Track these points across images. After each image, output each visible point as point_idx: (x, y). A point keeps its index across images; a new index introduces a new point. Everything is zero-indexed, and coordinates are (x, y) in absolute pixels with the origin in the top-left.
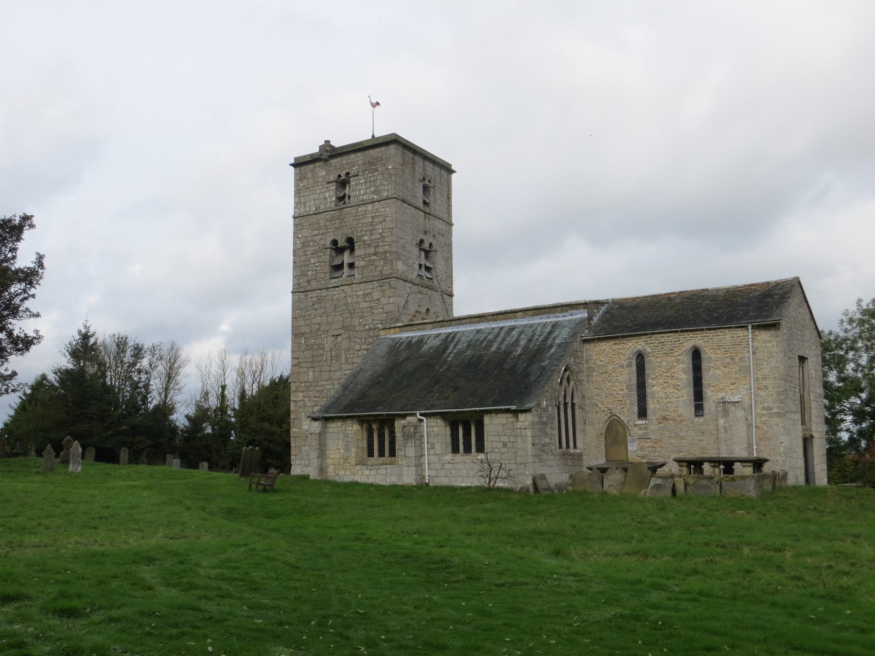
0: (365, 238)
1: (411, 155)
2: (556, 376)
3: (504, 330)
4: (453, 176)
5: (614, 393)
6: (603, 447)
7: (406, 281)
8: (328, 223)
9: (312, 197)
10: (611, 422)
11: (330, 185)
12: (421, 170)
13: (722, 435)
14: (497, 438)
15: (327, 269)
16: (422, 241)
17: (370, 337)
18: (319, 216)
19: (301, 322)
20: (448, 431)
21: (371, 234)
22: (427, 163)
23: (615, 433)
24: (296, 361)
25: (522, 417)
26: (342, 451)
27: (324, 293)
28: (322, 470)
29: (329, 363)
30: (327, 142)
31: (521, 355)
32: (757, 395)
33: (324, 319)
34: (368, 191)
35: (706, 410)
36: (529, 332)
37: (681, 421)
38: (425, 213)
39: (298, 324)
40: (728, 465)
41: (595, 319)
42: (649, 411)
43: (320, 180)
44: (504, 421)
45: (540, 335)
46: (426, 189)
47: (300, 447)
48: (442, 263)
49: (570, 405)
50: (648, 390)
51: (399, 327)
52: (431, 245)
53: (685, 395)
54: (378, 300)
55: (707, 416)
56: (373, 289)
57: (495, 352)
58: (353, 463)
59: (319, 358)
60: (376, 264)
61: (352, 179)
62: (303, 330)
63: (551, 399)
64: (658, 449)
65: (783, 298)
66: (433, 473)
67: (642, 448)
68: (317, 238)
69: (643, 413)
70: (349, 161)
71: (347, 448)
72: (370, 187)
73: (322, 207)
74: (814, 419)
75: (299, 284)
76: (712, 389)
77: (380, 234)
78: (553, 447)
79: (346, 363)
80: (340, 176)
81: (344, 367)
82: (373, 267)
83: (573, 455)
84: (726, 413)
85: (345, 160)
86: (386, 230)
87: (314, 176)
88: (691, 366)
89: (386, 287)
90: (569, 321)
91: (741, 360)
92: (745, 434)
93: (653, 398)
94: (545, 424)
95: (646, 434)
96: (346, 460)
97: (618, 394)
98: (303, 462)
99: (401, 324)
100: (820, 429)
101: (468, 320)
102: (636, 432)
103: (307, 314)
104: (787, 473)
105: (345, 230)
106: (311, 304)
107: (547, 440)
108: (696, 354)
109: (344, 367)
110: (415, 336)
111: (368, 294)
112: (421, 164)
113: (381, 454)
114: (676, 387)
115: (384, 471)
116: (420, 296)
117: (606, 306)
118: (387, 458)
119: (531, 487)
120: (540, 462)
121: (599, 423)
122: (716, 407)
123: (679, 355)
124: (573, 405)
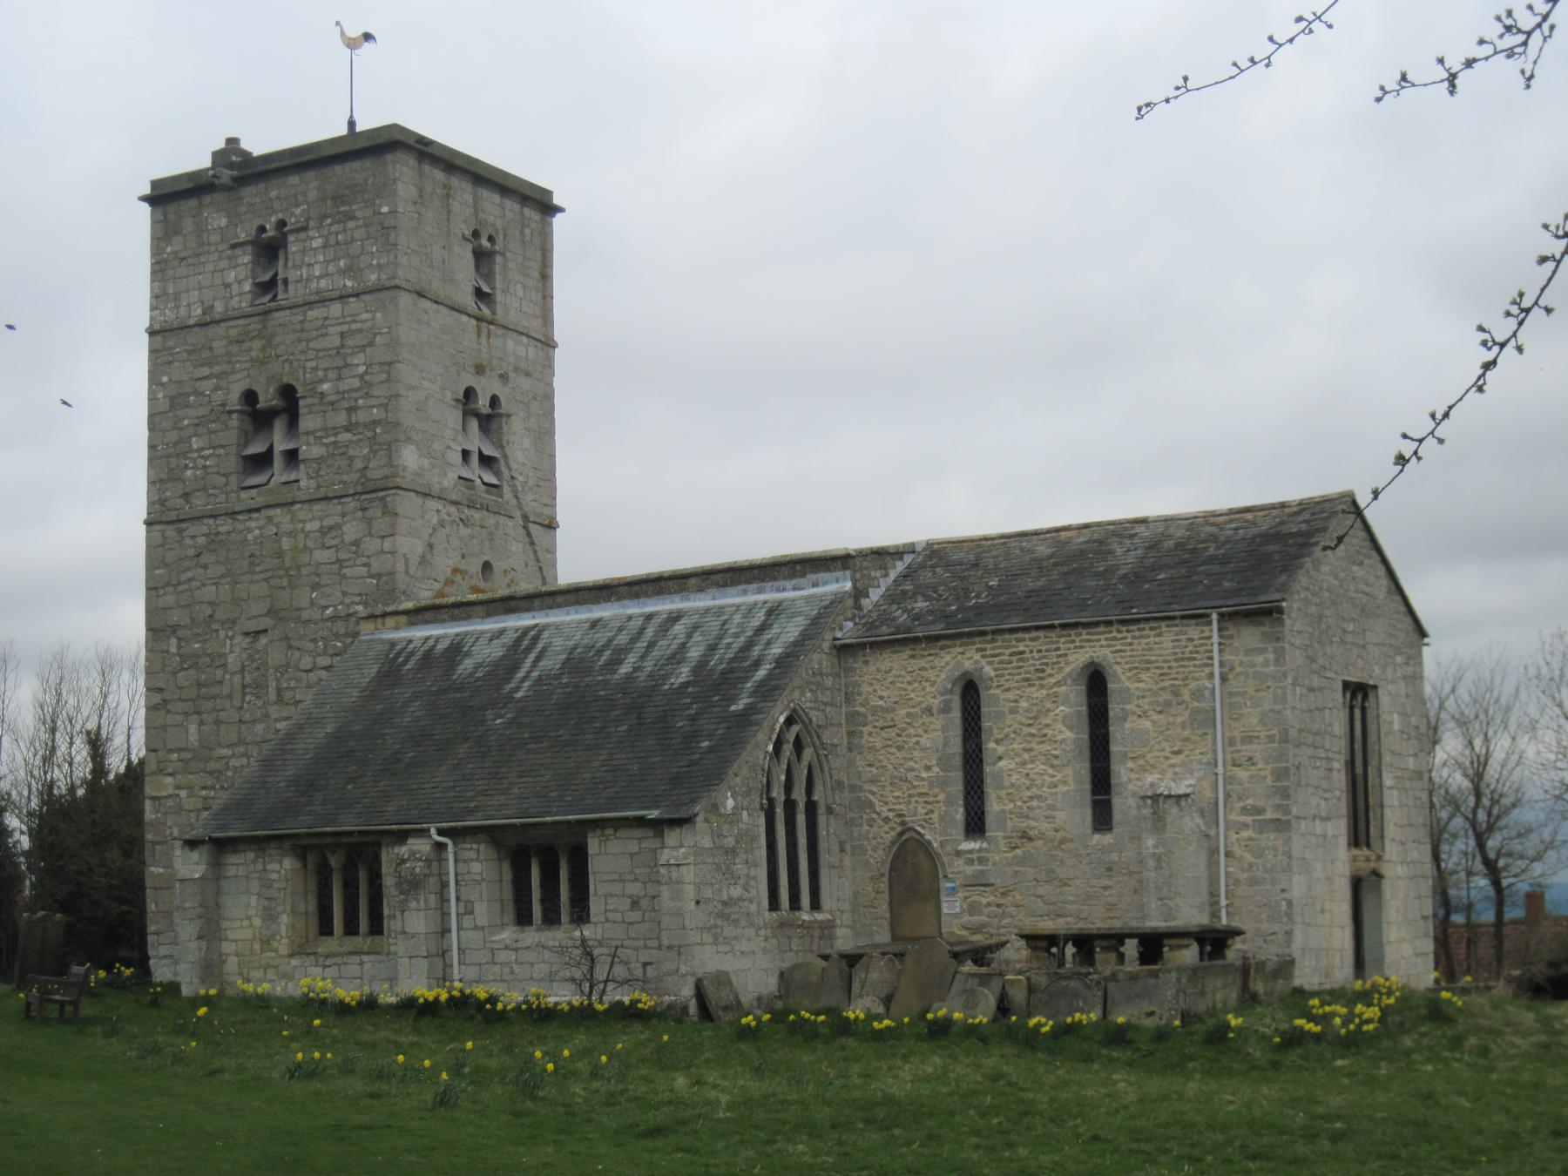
0: (325, 387)
1: (439, 175)
2: (761, 737)
3: (656, 621)
4: (558, 220)
5: (910, 776)
6: (885, 907)
7: (426, 495)
8: (234, 349)
9: (193, 281)
10: (903, 846)
11: (238, 251)
12: (469, 212)
14: (616, 888)
15: (232, 464)
16: (469, 393)
17: (337, 636)
18: (211, 331)
19: (169, 599)
20: (508, 875)
21: (339, 378)
22: (485, 193)
23: (911, 871)
24: (157, 698)
25: (672, 837)
26: (257, 922)
27: (224, 526)
28: (210, 969)
30: (232, 142)
31: (686, 685)
32: (1229, 780)
34: (331, 269)
35: (1117, 816)
36: (714, 625)
37: (1063, 841)
38: (479, 319)
39: (161, 603)
40: (1152, 946)
41: (875, 595)
42: (990, 819)
43: (214, 238)
44: (633, 847)
45: (736, 635)
46: (482, 258)
48: (526, 443)
49: (801, 806)
50: (987, 769)
51: (406, 612)
52: (494, 401)
53: (1070, 779)
54: (356, 543)
55: (1117, 830)
57: (629, 678)
58: (283, 950)
59: (215, 690)
60: (351, 452)
61: (291, 238)
62: (175, 617)
63: (748, 794)
65: (1303, 545)
66: (471, 972)
67: (973, 909)
69: (976, 824)
70: (284, 192)
71: (269, 916)
72: (336, 259)
73: (219, 307)
74: (1391, 831)
75: (162, 502)
76: (1130, 765)
77: (361, 377)
78: (753, 908)
79: (280, 700)
80: (262, 229)
81: (274, 712)
82: (344, 462)
84: (1158, 821)
85: (275, 190)
86: (376, 368)
87: (200, 229)
88: (1084, 709)
89: (375, 512)
94: (731, 852)
95: (982, 872)
96: (266, 942)
97: (918, 778)
99: (410, 605)
100: (1415, 855)
101: (572, 597)
102: (958, 869)
103: (184, 577)
104: (1292, 962)
105: (275, 367)
107: (736, 892)
108: (1096, 683)
109: (274, 712)
110: (444, 637)
111: (331, 528)
112: (469, 198)
113: (351, 929)
114: (1049, 760)
116: (465, 532)
117: (908, 559)
120: (715, 943)
121: (875, 849)
122: (1139, 808)
123: (1058, 684)
124: (811, 807)
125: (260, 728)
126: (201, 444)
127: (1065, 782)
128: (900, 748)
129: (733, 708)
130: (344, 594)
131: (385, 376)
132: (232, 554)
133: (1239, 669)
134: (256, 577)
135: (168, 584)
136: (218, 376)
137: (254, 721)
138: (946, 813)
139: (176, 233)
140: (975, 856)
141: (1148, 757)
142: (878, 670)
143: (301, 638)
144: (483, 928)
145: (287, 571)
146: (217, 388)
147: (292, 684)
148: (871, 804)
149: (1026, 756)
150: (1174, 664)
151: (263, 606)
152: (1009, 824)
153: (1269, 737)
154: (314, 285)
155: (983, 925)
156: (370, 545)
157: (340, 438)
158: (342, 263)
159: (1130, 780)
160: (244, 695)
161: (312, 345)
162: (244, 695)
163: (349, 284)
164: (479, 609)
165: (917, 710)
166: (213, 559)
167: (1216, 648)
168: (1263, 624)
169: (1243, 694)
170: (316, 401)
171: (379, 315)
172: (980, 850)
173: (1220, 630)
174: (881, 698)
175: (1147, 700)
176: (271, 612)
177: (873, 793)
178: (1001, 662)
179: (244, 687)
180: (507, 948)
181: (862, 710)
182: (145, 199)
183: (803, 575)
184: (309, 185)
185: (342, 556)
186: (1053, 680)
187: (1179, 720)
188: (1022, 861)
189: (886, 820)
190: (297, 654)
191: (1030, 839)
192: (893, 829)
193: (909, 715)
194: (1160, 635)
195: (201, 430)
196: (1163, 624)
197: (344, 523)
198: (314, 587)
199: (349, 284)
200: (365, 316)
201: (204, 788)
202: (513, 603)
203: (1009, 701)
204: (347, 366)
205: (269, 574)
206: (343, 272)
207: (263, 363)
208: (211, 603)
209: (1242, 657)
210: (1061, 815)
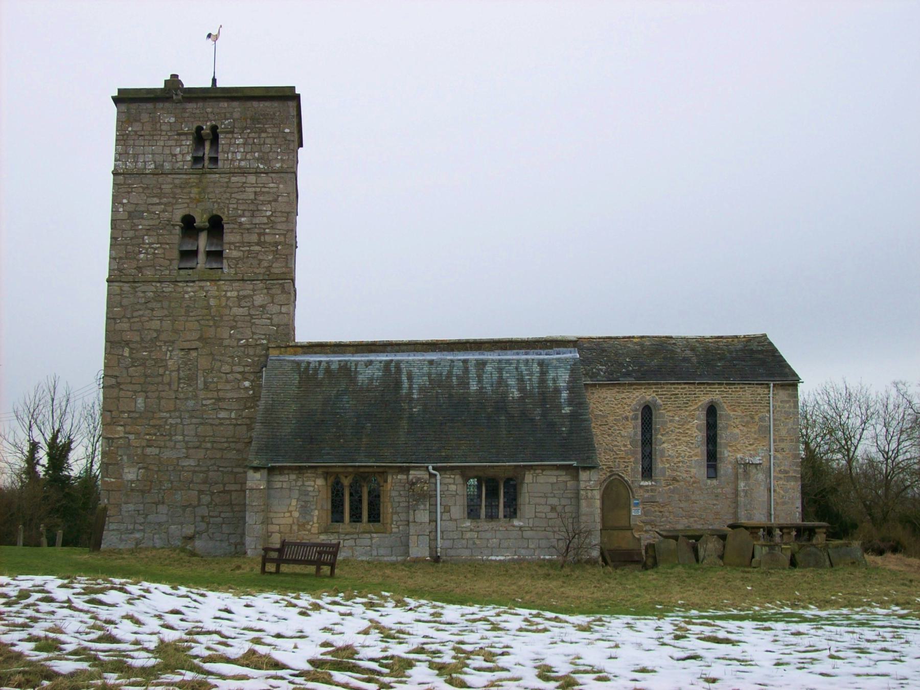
0: (243, 219)
5: (615, 449)
8: (179, 191)
10: (611, 482)
11: (183, 137)
13: (741, 499)
14: (543, 501)
15: (176, 254)
17: (248, 356)
21: (253, 216)
26: (296, 514)
29: (175, 387)
33: (167, 324)
37: (694, 482)
39: (118, 327)
47: (118, 506)
56: (254, 290)
58: (314, 530)
66: (448, 543)
68: (158, 209)
69: (647, 472)
71: (305, 509)
72: (252, 152)
73: (167, 166)
75: (120, 270)
76: (729, 449)
77: (268, 217)
79: (206, 387)
81: (202, 394)
82: (255, 262)
87: (155, 121)
89: (276, 290)
92: (765, 498)
93: (662, 456)
98: (123, 527)
101: (318, 349)
106: (143, 300)
108: (712, 411)
109: (202, 394)
111: (245, 297)
113: (356, 517)
115: (368, 542)
118: (364, 524)
119: (600, 559)
125: (191, 403)
126: (152, 240)
127: (696, 456)
130: (253, 333)
131: (284, 219)
132: (173, 304)
134: (190, 319)
135: (124, 317)
136: (165, 204)
137: (187, 399)
139: (136, 121)
143: (222, 355)
144: (456, 520)
145: (213, 317)
146: (164, 211)
147: (215, 380)
149: (677, 442)
151: (196, 335)
154: (237, 164)
156: (274, 309)
157: (252, 248)
158: (256, 154)
160: (179, 383)
161: (233, 195)
162: (179, 383)
163: (261, 166)
164: (351, 348)
166: (159, 305)
170: (236, 226)
171: (281, 186)
174: (601, 411)
176: (200, 339)
179: (179, 379)
180: (471, 530)
182: (114, 99)
183: (552, 348)
184: (237, 108)
185: (252, 312)
188: (673, 491)
190: (219, 364)
191: (677, 481)
193: (615, 420)
195: (150, 233)
196: (746, 386)
197: (254, 295)
198: (232, 328)
199: (261, 166)
200: (272, 185)
201: (148, 434)
202: (373, 348)
204: (258, 210)
205: (200, 318)
206: (258, 160)
207: (199, 201)
208: (155, 330)
209: (779, 403)
210: (693, 471)
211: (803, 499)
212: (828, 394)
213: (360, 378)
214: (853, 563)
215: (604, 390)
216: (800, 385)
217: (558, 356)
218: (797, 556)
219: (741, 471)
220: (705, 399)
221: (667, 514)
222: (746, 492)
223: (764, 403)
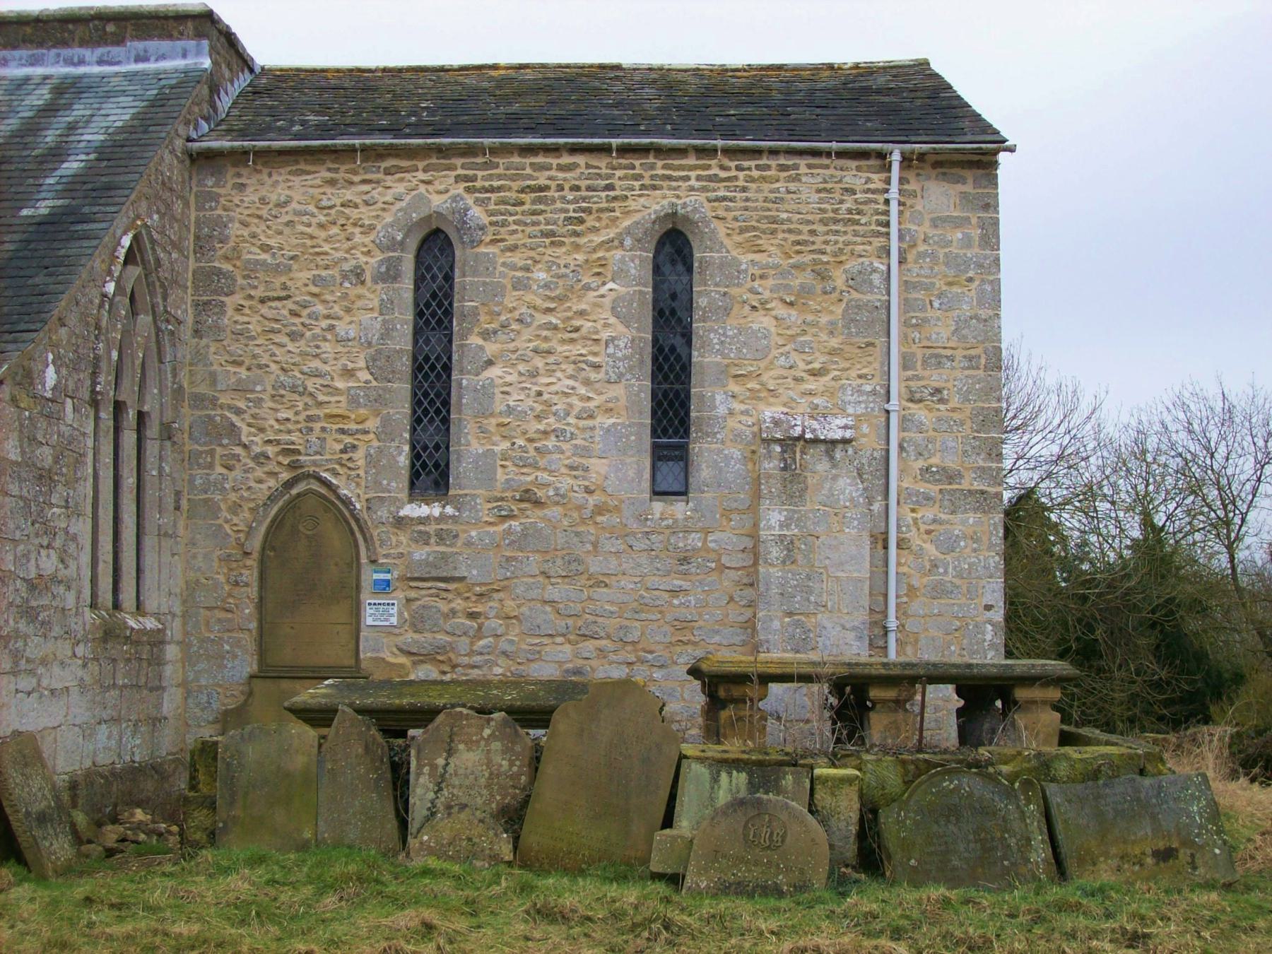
10: (293, 505)
13: (772, 573)
23: (306, 547)
32: (905, 422)
35: (703, 471)
37: (600, 510)
64: (494, 623)
69: (431, 472)
76: (733, 387)
83: (134, 639)
84: (792, 474)
90: (130, 77)
91: (857, 281)
92: (862, 570)
95: (444, 557)
107: (49, 563)
108: (674, 246)
121: (235, 508)
128: (293, 336)
129: (25, 212)
133: (922, 248)
138: (380, 450)
140: (431, 528)
141: (765, 378)
142: (263, 201)
148: (233, 430)
149: (539, 362)
150: (821, 228)
152: (500, 475)
153: (970, 358)
155: (441, 649)
159: (731, 412)
165: (335, 272)
167: (894, 208)
168: (962, 180)
169: (928, 288)
172: (443, 518)
173: (902, 180)
174: (266, 248)
175: (770, 282)
177: (238, 412)
178: (504, 202)
181: (227, 267)
186: (598, 239)
187: (824, 319)
188: (521, 541)
189: (261, 458)
191: (538, 503)
192: (272, 474)
194: (797, 179)
196: (802, 162)
203: (514, 267)
209: (926, 228)
210: (598, 467)
211: (1008, 573)
212: (1185, 407)
213: (1152, 641)
214: (1165, 855)
215: (281, 175)
216: (1003, 157)
217: (141, 66)
218: (888, 820)
219: (771, 466)
220: (653, 205)
221: (494, 623)
222: (789, 546)
223: (868, 220)
